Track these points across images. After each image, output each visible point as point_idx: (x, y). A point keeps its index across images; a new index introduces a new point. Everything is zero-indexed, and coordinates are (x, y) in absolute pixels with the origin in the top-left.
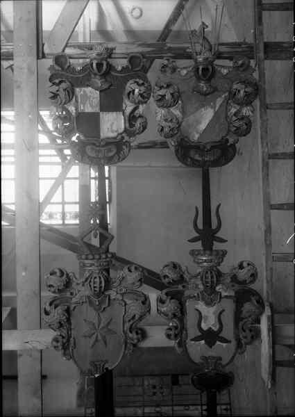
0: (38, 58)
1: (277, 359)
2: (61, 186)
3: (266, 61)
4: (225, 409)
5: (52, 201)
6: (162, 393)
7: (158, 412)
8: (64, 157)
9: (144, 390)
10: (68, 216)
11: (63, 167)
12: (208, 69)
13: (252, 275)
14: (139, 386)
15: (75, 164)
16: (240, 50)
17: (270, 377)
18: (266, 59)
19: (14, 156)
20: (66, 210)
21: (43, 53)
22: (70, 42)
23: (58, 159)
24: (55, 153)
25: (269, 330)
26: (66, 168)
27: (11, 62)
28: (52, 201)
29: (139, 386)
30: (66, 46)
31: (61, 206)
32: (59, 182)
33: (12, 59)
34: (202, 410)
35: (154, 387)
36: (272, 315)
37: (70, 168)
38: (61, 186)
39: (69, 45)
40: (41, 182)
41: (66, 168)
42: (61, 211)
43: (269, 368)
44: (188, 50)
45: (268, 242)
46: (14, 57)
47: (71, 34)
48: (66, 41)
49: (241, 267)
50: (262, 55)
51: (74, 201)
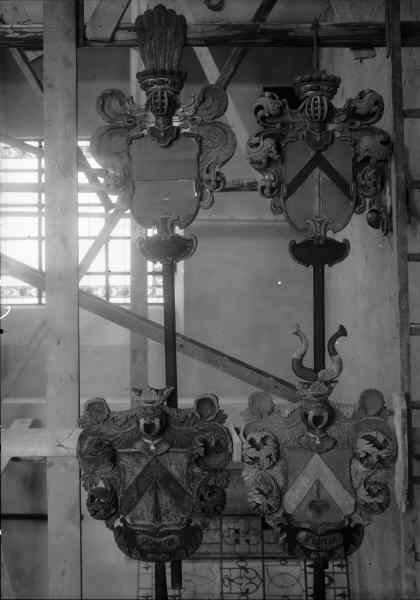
0: (78, 45)
1: (415, 474)
2: (104, 247)
3: (403, 49)
4: (339, 566)
5: (93, 241)
6: (248, 541)
7: (242, 568)
8: (108, 205)
9: (222, 536)
10: (114, 292)
11: (107, 220)
12: (322, 418)
13: (376, 103)
14: (216, 530)
15: (126, 216)
16: (366, 32)
17: (406, 496)
18: (403, 45)
19: (39, 188)
20: (111, 283)
21: (85, 39)
22: (123, 21)
23: (102, 210)
24: (98, 201)
25: (403, 430)
26: (111, 222)
27: (39, 53)
28: (93, 241)
29: (216, 530)
30: (117, 28)
31: (103, 278)
32: (103, 240)
33: (41, 48)
34: (306, 566)
35: (237, 531)
36: (408, 410)
37: (117, 220)
38: (104, 247)
39: (123, 26)
40: (81, 242)
41: (111, 222)
42: (104, 284)
43: (404, 483)
44: (292, 34)
45: (403, 307)
46: (45, 45)
47: (123, 15)
48: (117, 20)
49: (362, 95)
50: (398, 38)
51: (122, 270)
